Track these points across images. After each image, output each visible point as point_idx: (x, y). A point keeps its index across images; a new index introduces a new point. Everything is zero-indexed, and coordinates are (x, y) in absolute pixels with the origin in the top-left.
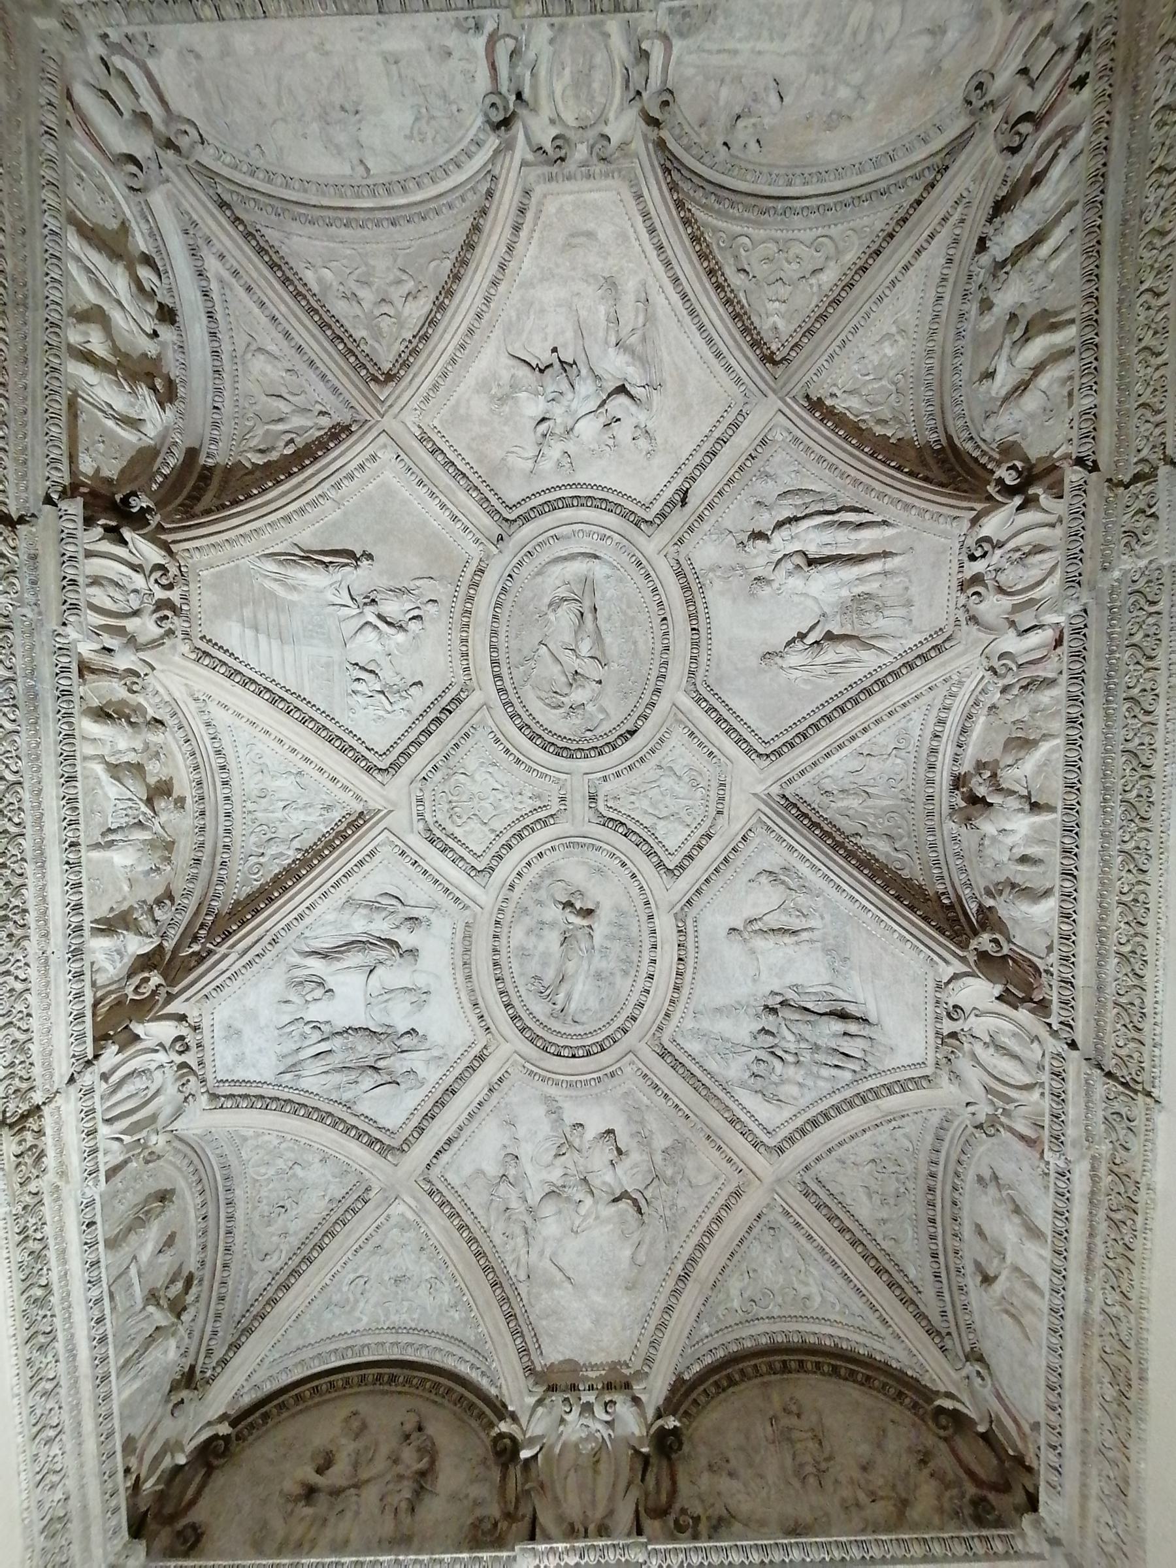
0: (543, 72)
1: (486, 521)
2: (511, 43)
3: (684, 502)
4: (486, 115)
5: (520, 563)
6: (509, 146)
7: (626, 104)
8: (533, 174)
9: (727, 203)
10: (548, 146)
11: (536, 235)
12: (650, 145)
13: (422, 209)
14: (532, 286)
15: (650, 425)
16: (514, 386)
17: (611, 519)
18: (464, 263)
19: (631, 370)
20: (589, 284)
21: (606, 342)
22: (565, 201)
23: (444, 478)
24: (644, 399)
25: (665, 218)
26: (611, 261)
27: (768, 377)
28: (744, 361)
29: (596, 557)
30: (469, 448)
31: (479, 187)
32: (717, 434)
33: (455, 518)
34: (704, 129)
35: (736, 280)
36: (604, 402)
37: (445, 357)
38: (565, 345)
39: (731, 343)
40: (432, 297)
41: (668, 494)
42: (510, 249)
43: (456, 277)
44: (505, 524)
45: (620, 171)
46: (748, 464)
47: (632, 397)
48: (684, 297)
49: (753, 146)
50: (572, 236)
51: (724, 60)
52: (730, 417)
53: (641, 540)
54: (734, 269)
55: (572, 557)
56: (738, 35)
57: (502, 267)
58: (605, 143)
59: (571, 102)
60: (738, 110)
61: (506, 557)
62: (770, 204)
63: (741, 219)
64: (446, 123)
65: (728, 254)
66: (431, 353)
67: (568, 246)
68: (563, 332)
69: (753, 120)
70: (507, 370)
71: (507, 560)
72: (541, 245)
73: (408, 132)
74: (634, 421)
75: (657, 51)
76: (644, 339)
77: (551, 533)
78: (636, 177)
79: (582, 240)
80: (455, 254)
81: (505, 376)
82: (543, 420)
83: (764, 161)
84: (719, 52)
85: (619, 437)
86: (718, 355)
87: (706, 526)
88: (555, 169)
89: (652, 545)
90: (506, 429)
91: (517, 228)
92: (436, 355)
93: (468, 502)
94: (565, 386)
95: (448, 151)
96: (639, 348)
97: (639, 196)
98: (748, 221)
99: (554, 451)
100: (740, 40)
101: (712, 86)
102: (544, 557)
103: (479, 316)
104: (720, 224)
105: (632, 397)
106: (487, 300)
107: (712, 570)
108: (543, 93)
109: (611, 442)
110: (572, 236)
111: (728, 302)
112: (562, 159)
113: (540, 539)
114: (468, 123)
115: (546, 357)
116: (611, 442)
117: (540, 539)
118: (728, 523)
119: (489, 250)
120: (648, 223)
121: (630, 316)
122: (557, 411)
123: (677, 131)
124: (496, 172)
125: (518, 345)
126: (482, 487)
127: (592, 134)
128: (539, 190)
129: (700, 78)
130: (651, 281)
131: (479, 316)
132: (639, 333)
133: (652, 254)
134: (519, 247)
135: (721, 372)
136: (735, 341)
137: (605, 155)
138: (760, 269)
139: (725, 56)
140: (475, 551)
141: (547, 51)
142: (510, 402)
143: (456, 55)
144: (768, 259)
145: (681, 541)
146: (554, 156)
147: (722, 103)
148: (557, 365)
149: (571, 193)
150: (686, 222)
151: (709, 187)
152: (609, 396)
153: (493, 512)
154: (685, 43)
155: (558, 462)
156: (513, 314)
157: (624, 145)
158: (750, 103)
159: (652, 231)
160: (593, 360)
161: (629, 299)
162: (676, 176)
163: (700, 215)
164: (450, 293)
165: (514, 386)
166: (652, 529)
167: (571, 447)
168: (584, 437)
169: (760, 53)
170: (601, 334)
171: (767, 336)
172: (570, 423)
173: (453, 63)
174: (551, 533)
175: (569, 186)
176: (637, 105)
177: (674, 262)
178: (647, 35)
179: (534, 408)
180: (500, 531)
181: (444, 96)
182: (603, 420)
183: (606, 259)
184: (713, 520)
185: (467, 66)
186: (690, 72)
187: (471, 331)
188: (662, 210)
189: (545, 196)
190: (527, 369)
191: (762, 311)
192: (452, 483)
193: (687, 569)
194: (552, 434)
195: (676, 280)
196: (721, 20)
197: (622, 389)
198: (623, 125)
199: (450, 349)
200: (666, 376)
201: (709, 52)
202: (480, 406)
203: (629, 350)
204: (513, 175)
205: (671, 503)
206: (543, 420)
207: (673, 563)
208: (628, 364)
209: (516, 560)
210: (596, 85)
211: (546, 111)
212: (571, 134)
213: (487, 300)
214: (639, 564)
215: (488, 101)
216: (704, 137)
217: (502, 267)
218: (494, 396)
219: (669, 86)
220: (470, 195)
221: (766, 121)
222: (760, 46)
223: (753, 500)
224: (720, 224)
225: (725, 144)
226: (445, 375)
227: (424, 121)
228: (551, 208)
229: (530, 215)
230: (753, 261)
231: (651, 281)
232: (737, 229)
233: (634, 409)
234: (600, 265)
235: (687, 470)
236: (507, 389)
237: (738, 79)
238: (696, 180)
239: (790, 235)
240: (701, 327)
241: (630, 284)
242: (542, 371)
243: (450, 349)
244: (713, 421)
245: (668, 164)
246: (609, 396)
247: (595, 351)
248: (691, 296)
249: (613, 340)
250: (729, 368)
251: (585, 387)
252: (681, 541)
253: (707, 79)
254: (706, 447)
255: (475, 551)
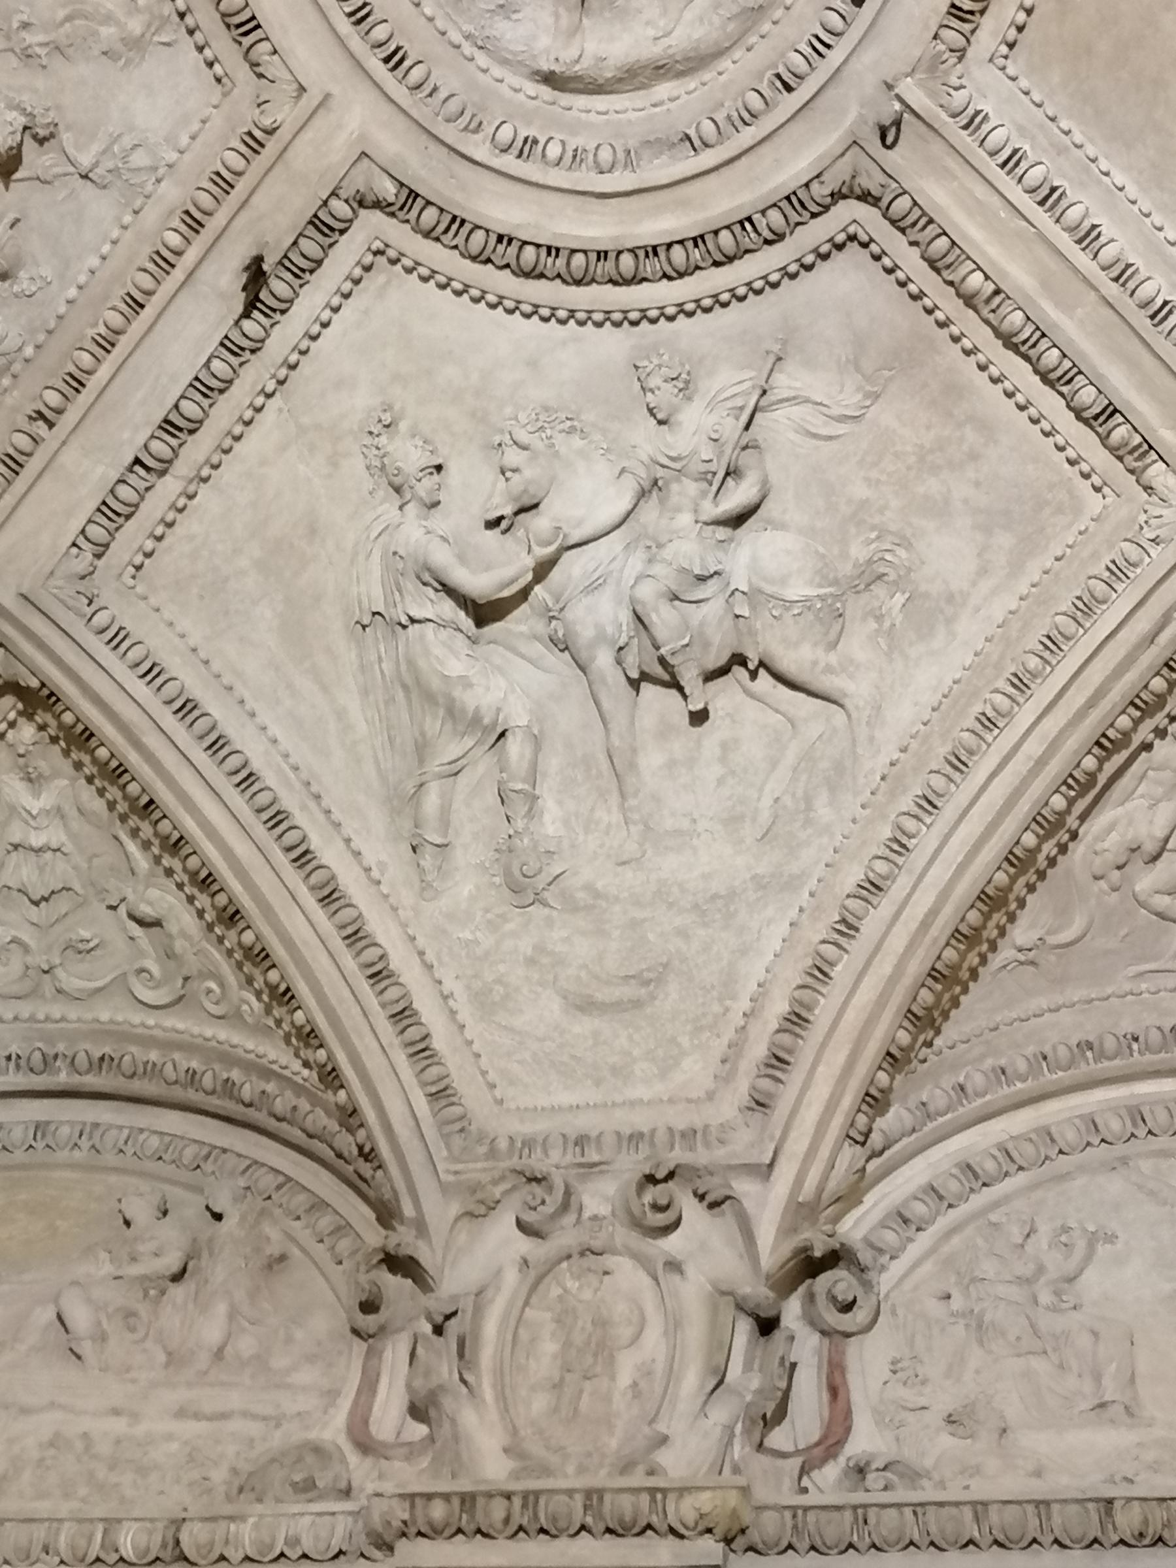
0: (692, 1381)
1: (938, 195)
2: (778, 1438)
3: (256, 274)
4: (867, 1285)
5: (820, 47)
6: (802, 1211)
7: (467, 1305)
8: (745, 1143)
9: (207, 1081)
10: (691, 1209)
11: (745, 1005)
12: (408, 1210)
13: (1090, 1067)
14: (760, 883)
15: (389, 509)
16: (830, 616)
17: (500, 209)
18: (966, 937)
19: (455, 667)
20: (589, 887)
21: (537, 742)
22: (673, 1083)
23: (1076, 330)
24: (410, 585)
25: (365, 1045)
26: (525, 946)
27: (27, 648)
28: (104, 690)
29: (550, 79)
30: (986, 427)
31: (908, 1120)
32: (169, 487)
33: (1049, 197)
34: (274, 1250)
35: (163, 899)
36: (542, 570)
37: (1043, 693)
38: (664, 732)
39: (152, 740)
40: (1078, 851)
41: (310, 302)
42: (821, 972)
43: (994, 901)
44: (871, 181)
45: (493, 1153)
46: (53, 398)
47: (450, 591)
48: (303, 858)
49: (140, 1210)
50: (637, 1004)
51: (210, 1399)
52: (131, 538)
53: (398, 147)
54: (172, 927)
55: (634, 77)
56: (174, 1446)
57: (848, 927)
58: (529, 1217)
59: (621, 1309)
60: (177, 1292)
61: (869, 67)
62: (92, 1081)
63: (167, 1045)
64: (988, 1268)
65: (193, 964)
66: (1091, 704)
67: (650, 980)
68: (671, 764)
69: (135, 1270)
70: (856, 662)
71: (867, 57)
72: (729, 983)
73: (1102, 1250)
74: (439, 522)
75: (389, 1415)
76: (422, 749)
77: (708, 158)
78: (446, 1137)
79: (604, 994)
80: (996, 961)
81: (858, 643)
82: (738, 520)
83: (113, 1179)
84: (224, 1416)
85: (488, 476)
86: (186, 709)
87: (172, 194)
88: (677, 1156)
89: (351, 126)
90: (860, 491)
91: (797, 1020)
92: (1077, 698)
93: (996, 249)
94: (664, 619)
95: (996, 1205)
96: (433, 725)
97: (441, 1094)
98: (147, 1042)
99: (700, 427)
100: (170, 1437)
101: (246, 1345)
102: (736, 73)
103: (929, 803)
104: (223, 1033)
105: (450, 591)
106: (899, 845)
107: (136, 45)
108: (695, 1334)
109: (513, 457)
110: (637, 1004)
111: (176, 845)
112: (651, 1179)
113: (749, 135)
114: (928, 1267)
115: (724, 698)
116: (513, 457)
117: (749, 135)
118: (100, 208)
119: (884, 967)
120: (413, 1033)
121: (471, 813)
122: (688, 547)
123: (344, 1245)
124: (850, 1155)
125: (814, 730)
126: (949, 305)
127: (566, 1237)
128: (728, 1107)
129: (279, 1362)
130: (406, 897)
131: (929, 803)
132: (434, 766)
133: (400, 960)
134: (792, 974)
135: (175, 664)
136: (138, 745)
137: (535, 1190)
138: (98, 924)
139: (208, 1408)
140: (985, 85)
141: (673, 1424)
142: (847, 569)
143: (934, 1418)
144: (81, 950)
145: (254, 144)
146: (664, 1189)
147: (222, 1308)
148: (689, 677)
149: (633, 1104)
150: (309, 1036)
151: (259, 1117)
152: (524, 594)
153: (914, 223)
154: (313, 1435)
155: (686, 387)
156: (823, 812)
157: (480, 1209)
158: (143, 1309)
159: (403, 1015)
160: (578, 686)
161: (471, 853)
162: (346, 1142)
163: (277, 1053)
164: (1017, 861)
165: (830, 616)
166: (357, 183)
167: (645, 440)
168: (603, 469)
169: (116, 1412)
170: (552, 763)
171: (52, 759)
172: (650, 512)
173: (944, 1401)
174: (708, 158)
175: (640, 1121)
176: (437, 1303)
177: (338, 944)
178: (412, 1451)
179: (769, 556)
180: (893, 159)
181: (980, 1328)
182: (540, 523)
183: (540, 948)
184: (151, 216)
185: (909, 1396)
186: (306, 1376)
187: (958, 764)
188: (374, 1063)
189: (710, 1096)
190: (787, 663)
191: (76, 824)
192: (1051, 313)
193: (223, 45)
194: (706, 477)
195: (330, 897)
196: (219, 1475)
197: (484, 612)
198: (481, 1258)
199: (1026, 716)
200: (348, 655)
201: (246, 1414)
202: (946, 555)
203: (457, 717)
204: (797, 1145)
205: (302, 271)
206: (738, 520)
207: (273, 66)
208: (466, 682)
209: (835, 57)
210: (549, 1347)
211: (692, 1291)
212: (623, 1235)
213: (899, 845)
214: (394, 59)
215: (860, 1316)
216: (272, 1232)
217: (848, 927)
218: (896, 586)
219: (360, 1347)
220: (939, 1100)
221: (107, 1269)
222: (119, 1425)
223: (23, 283)
224: (223, 1033)
225: (218, 1217)
226: (1051, 643)
227: (1052, 1273)
228: (695, 1071)
229: (758, 1050)
230: (120, 943)
231: (406, 897)
232: (174, 1022)
233: (442, 558)
234: (558, 934)
235: (256, 374)
236: (854, 606)
237: (174, 1360)
238: (297, 1135)
239: (25, 1009)
240: (247, 780)
241: (467, 889)
242: (739, 659)
243: (1026, 716)
244: (187, 525)
245: (366, 1169)
246: (524, 594)
247: (571, 716)
248: (282, 860)
249: (515, 747)
250: (152, 673)
251: (599, 616)
252: (254, 144)
253: (260, 1361)
254: (197, 449)
255: (985, 85)
